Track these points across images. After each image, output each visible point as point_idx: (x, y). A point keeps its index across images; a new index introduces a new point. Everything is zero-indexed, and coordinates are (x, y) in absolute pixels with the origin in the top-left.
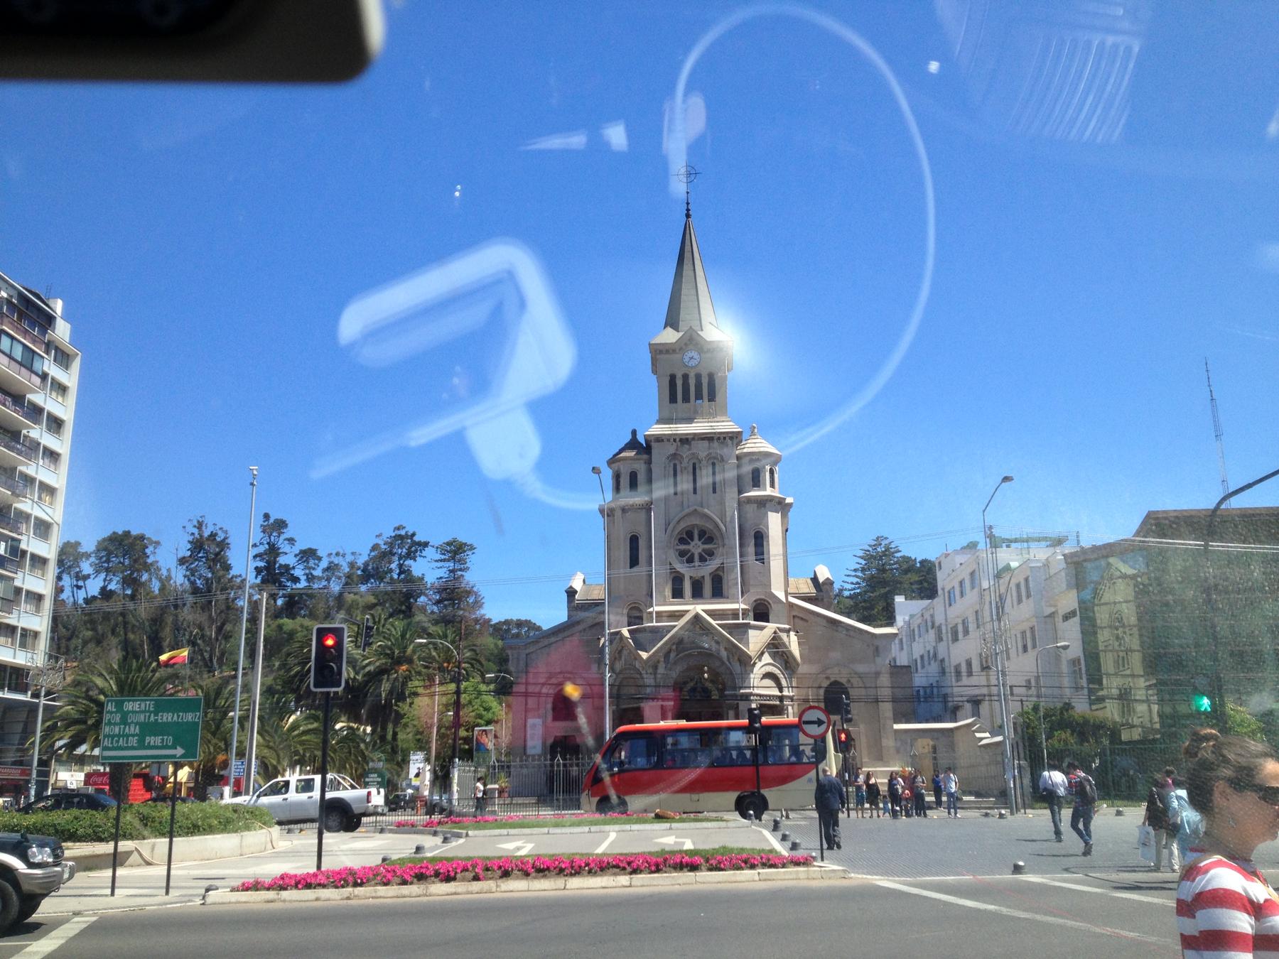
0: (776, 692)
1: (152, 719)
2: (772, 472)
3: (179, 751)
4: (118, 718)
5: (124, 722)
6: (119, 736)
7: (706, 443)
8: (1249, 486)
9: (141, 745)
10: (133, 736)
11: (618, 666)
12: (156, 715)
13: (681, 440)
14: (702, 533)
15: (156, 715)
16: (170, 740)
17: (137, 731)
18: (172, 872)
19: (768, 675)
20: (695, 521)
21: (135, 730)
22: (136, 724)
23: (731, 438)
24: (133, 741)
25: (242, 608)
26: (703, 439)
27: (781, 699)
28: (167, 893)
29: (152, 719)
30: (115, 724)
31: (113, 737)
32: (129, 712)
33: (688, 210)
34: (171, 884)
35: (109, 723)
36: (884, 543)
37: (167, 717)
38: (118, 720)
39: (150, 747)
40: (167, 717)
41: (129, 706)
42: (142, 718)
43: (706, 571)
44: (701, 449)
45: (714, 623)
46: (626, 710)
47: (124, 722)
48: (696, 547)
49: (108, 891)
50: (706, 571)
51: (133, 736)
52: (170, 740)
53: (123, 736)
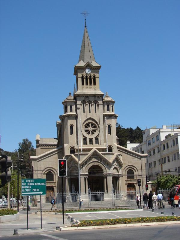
0: (117, 173)
1: (34, 184)
2: (113, 107)
3: (41, 193)
4: (25, 184)
5: (27, 185)
6: (26, 189)
7: (93, 98)
8: (83, 46)
9: (32, 191)
10: (30, 189)
11: (70, 165)
12: (35, 183)
13: (86, 96)
14: (92, 124)
15: (35, 183)
16: (39, 190)
17: (30, 187)
18: (29, 224)
19: (115, 168)
20: (90, 121)
21: (29, 187)
22: (30, 186)
23: (101, 96)
24: (29, 190)
25: (63, 158)
26: (92, 96)
27: (118, 175)
28: (41, 228)
29: (34, 184)
30: (24, 186)
31: (24, 189)
32: (28, 183)
33: (85, 25)
34: (42, 226)
35: (23, 186)
36: (118, 124)
37: (37, 184)
38: (25, 185)
39: (34, 192)
40: (37, 184)
41: (28, 181)
42: (31, 184)
43: (93, 136)
44: (92, 99)
45: (100, 153)
46: (72, 178)
47: (27, 185)
48: (91, 128)
49: (41, 228)
50: (93, 136)
51: (30, 189)
52: (39, 190)
53: (27, 189)
